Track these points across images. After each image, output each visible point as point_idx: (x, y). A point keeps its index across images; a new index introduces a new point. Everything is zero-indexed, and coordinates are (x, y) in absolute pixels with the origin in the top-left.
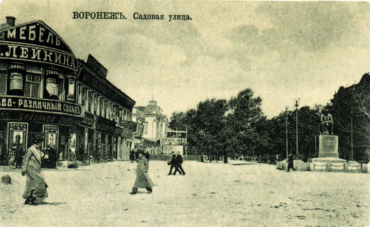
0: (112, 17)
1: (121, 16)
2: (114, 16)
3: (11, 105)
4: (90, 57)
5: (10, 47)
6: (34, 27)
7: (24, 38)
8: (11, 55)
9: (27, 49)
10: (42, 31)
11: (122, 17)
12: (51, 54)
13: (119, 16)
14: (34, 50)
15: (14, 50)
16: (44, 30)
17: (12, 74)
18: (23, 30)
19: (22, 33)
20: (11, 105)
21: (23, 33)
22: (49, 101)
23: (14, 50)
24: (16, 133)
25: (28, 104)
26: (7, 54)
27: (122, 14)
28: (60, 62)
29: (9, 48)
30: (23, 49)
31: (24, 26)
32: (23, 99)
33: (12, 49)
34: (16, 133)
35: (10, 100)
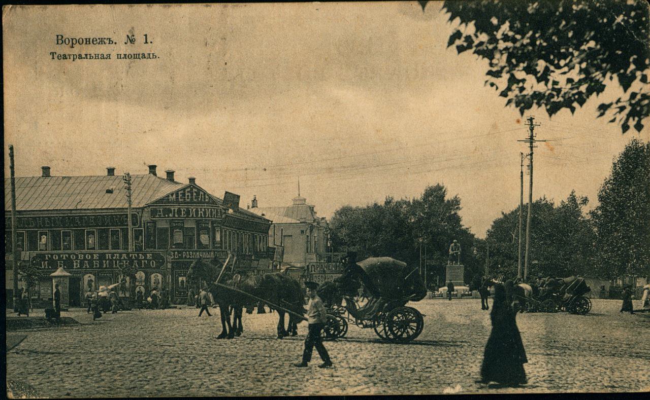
0: (101, 43)
1: (110, 41)
2: (102, 41)
3: (177, 257)
4: (192, 180)
5: (172, 209)
6: (189, 190)
7: (182, 200)
8: (174, 216)
9: (185, 209)
10: (195, 192)
11: (111, 42)
12: (203, 210)
13: (107, 42)
14: (190, 210)
15: (176, 211)
16: (196, 190)
17: (175, 230)
18: (181, 194)
19: (180, 196)
20: (177, 257)
21: (181, 195)
22: (204, 251)
23: (176, 211)
24: (180, 279)
25: (190, 255)
26: (171, 215)
27: (111, 40)
28: (203, 216)
29: (171, 210)
30: (182, 210)
31: (181, 190)
32: (186, 252)
33: (174, 210)
34: (180, 279)
35: (176, 253)
